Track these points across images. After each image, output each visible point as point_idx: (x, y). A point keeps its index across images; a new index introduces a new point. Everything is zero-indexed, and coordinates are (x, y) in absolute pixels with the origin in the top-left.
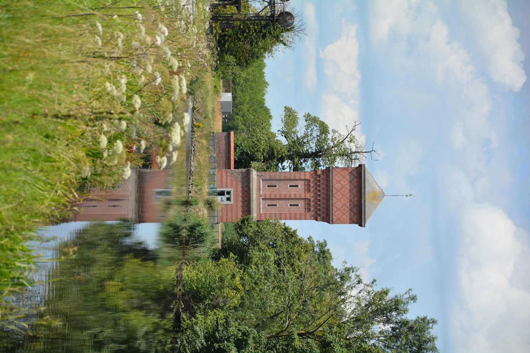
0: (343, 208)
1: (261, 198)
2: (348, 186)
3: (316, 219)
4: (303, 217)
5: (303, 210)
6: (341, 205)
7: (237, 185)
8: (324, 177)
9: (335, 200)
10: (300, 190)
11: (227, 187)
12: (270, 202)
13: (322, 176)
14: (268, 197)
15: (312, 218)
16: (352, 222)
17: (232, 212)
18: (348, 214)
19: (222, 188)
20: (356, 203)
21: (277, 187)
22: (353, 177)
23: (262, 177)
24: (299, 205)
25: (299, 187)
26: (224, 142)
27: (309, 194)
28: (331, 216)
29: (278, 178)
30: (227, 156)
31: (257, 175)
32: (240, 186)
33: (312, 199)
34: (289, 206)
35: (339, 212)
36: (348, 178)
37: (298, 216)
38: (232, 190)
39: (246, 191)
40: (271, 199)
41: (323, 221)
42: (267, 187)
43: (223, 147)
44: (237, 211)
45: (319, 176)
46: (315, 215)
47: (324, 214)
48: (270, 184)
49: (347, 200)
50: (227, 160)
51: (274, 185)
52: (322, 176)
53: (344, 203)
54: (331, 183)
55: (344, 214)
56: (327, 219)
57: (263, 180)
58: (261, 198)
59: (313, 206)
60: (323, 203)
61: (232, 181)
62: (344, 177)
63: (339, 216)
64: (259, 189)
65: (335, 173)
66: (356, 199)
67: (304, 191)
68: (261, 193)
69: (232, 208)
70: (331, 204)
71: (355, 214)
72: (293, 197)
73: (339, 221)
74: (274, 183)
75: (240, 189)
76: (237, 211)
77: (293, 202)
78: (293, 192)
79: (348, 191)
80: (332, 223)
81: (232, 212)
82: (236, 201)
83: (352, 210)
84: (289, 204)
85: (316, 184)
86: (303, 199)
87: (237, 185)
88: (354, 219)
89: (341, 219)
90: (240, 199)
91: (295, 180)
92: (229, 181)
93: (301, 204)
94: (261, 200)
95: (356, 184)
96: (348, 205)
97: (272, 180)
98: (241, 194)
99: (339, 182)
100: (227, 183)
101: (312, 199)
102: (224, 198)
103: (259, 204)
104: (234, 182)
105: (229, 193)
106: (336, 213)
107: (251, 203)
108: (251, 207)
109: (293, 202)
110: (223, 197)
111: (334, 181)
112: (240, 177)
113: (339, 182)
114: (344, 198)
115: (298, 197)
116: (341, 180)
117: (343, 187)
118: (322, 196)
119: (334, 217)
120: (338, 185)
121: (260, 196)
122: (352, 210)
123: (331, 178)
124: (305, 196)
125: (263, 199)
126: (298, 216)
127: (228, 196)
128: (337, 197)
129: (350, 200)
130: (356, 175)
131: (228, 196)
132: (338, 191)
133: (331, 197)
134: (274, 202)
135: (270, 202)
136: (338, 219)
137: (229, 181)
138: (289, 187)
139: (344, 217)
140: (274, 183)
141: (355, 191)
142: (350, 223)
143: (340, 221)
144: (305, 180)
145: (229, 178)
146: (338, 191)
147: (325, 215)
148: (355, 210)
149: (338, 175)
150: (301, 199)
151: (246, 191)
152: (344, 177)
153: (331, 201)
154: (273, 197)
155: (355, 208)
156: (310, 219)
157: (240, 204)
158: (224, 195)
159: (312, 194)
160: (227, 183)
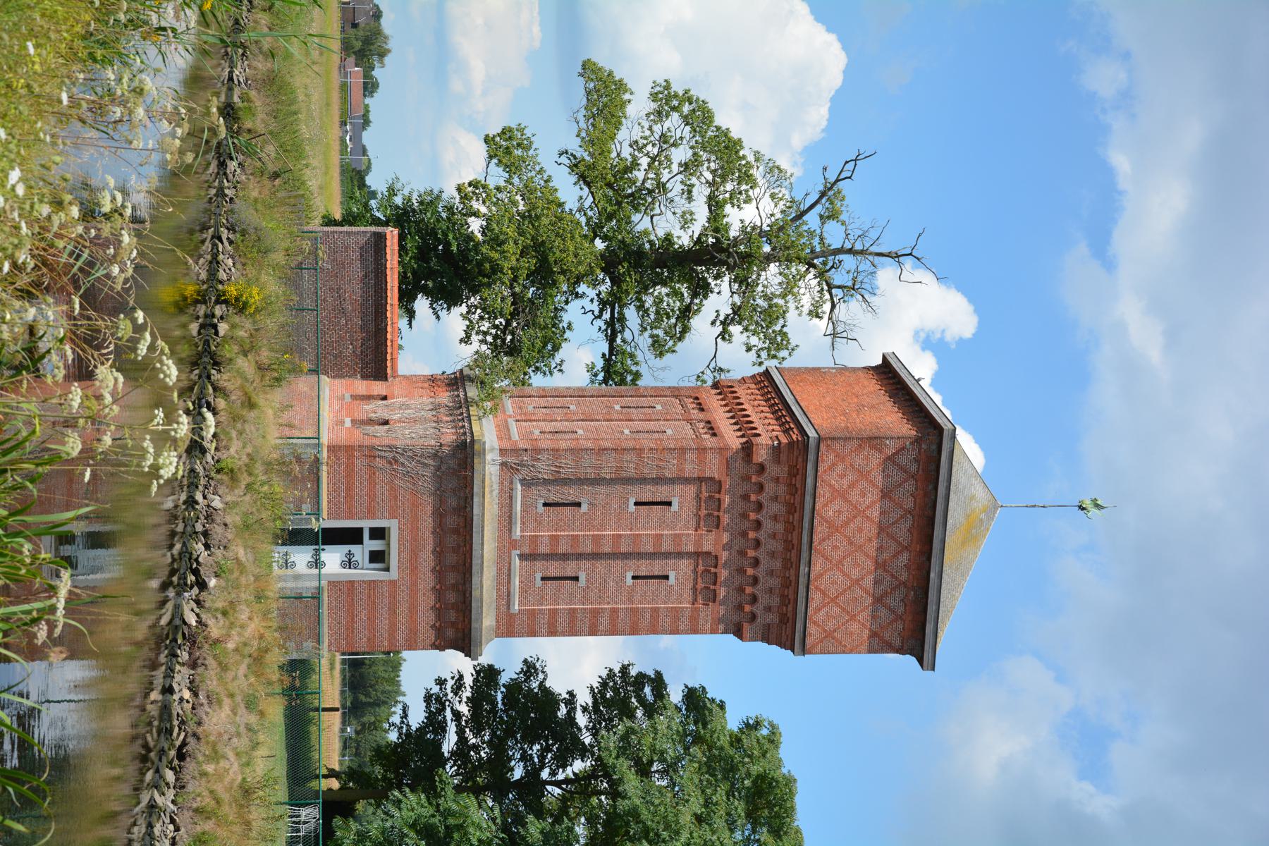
0: (849, 595)
1: (515, 553)
2: (874, 513)
3: (739, 633)
4: (685, 623)
5: (687, 594)
6: (843, 582)
7: (415, 506)
8: (783, 471)
9: (818, 565)
10: (679, 522)
11: (371, 514)
12: (552, 568)
13: (772, 469)
14: (544, 549)
15: (721, 627)
16: (879, 644)
17: (392, 610)
18: (865, 617)
19: (351, 516)
20: (903, 576)
21: (584, 508)
22: (898, 477)
23: (524, 472)
24: (672, 575)
25: (675, 507)
26: (356, 271)
27: (712, 536)
28: (799, 626)
29: (590, 473)
30: (372, 327)
31: (503, 464)
32: (429, 509)
33: (724, 556)
34: (629, 581)
35: (833, 609)
36: (877, 476)
37: (666, 621)
38: (393, 525)
39: (455, 531)
40: (559, 481)
41: (767, 639)
42: (541, 509)
43: (354, 290)
44: (413, 609)
45: (762, 468)
46: (734, 617)
47: (777, 618)
48: (553, 498)
49: (870, 565)
50: (371, 343)
51: (571, 499)
52: (772, 469)
53: (855, 574)
54: (808, 498)
55: (853, 618)
56: (786, 630)
57: (523, 481)
58: (515, 553)
59: (729, 491)
60: (772, 554)
61: (393, 490)
62: (865, 475)
63: (831, 626)
64: (507, 519)
65: (827, 458)
66: (904, 558)
67: (693, 522)
68: (517, 532)
69: (392, 596)
70: (802, 580)
71: (898, 617)
72: (646, 547)
73: (827, 643)
74: (570, 493)
75: (426, 522)
76: (413, 609)
77: (645, 568)
78: (649, 529)
79: (875, 530)
80: (804, 652)
81: (392, 610)
82: (411, 565)
83: (887, 600)
84: (629, 575)
85: (740, 607)
86: (688, 555)
87: (415, 506)
88: (891, 636)
89: (838, 635)
90: (427, 559)
91: (660, 480)
92: (382, 490)
93: (680, 573)
94: (517, 562)
95: (909, 504)
96: (869, 582)
97: (565, 482)
98: (430, 600)
99: (842, 494)
100: (372, 496)
101: (724, 556)
102: (360, 552)
103: (505, 577)
104: (403, 496)
105: (378, 533)
106: (820, 614)
107: (475, 580)
108: (475, 593)
109: (645, 568)
110: (355, 549)
111: (820, 491)
112: (428, 473)
113: (842, 494)
114: (858, 555)
115: (668, 547)
116: (852, 485)
117: (859, 512)
118: (768, 545)
119: (811, 628)
120: (839, 505)
121: (513, 544)
122: (887, 600)
123: (809, 481)
124: (698, 543)
125: (522, 557)
126: (666, 621)
127: (377, 545)
128: (829, 552)
129: (880, 565)
130: (913, 467)
131: (377, 545)
132: (834, 529)
133: (805, 555)
134: (568, 568)
135: (552, 568)
136: (828, 635)
137: (382, 490)
138: (632, 508)
139: (854, 627)
140: (570, 493)
141: (902, 530)
142: (872, 650)
143: (834, 644)
144: (700, 480)
145: (382, 477)
146: (834, 529)
147: (773, 618)
148: (896, 603)
149: (840, 468)
150: (679, 555)
151: (455, 531)
152: (865, 475)
153: (803, 569)
154: (565, 548)
155: (899, 595)
156: (714, 631)
157: (427, 581)
158: (360, 542)
159: (725, 537)
160: (372, 496)
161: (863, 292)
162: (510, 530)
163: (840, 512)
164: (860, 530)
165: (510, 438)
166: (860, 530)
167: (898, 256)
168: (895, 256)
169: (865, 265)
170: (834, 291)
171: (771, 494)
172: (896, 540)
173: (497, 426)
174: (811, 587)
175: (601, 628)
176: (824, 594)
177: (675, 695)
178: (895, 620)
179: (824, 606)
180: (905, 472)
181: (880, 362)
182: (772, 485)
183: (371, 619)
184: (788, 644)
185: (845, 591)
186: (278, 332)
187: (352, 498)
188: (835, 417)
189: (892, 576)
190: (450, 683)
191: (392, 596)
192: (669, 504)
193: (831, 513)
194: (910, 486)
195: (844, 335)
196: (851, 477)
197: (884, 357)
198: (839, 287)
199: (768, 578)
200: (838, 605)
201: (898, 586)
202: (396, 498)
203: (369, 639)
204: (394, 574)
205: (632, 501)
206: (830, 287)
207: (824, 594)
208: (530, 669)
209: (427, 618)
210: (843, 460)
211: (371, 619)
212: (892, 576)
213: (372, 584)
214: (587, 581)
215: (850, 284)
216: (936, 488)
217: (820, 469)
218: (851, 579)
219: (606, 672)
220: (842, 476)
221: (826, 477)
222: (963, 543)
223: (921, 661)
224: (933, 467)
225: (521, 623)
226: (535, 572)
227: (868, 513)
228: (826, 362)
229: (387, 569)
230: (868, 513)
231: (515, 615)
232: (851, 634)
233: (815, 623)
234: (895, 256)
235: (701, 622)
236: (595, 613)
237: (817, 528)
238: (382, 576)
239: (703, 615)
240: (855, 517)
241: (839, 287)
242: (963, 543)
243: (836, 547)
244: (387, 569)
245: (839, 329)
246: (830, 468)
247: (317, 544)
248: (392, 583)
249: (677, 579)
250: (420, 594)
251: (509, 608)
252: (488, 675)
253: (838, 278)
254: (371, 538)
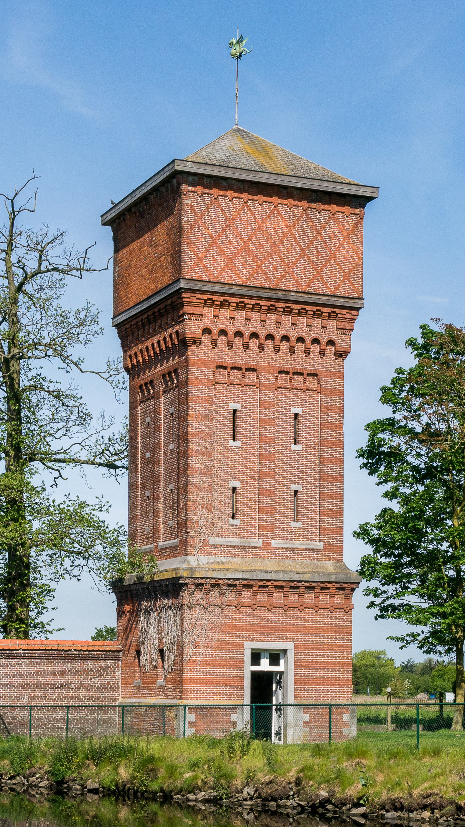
0: (314, 258)
6: (303, 263)
11: (240, 664)
17: (318, 647)
19: (242, 681)
20: (298, 211)
25: (237, 406)
35: (326, 272)
38: (250, 646)
44: (318, 630)
55: (333, 256)
63: (339, 275)
69: (308, 647)
73: (353, 279)
76: (318, 630)
81: (318, 647)
99: (230, 261)
111: (226, 279)
113: (230, 261)
116: (222, 252)
119: (341, 292)
120: (238, 263)
132: (259, 269)
136: (346, 278)
146: (259, 269)
157: (295, 618)
161: (45, 243)
162: (255, 548)
163: (244, 263)
164: (260, 246)
165: (177, 547)
166: (260, 246)
167: (14, 212)
168: (14, 215)
169: (23, 240)
170: (43, 269)
171: (228, 322)
172: (269, 216)
173: (165, 557)
174: (307, 290)
175: (337, 472)
176: (313, 279)
177: (386, 412)
178: (336, 219)
179: (323, 280)
180: (211, 205)
181: (109, 229)
182: (220, 321)
183: (326, 665)
184: (353, 312)
185: (310, 261)
186: (317, 794)
187: (226, 680)
188: (162, 266)
189: (298, 220)
190: (371, 598)
191: (308, 647)
192: (235, 411)
193: (245, 271)
194: (223, 202)
195: (81, 261)
196: (214, 251)
197: (105, 224)
198: (40, 265)
199: (298, 327)
200: (322, 269)
201: (308, 216)
202: (227, 643)
203: (342, 667)
204: (289, 646)
205: (231, 443)
206: (39, 272)
207: (313, 279)
208: (363, 532)
209: (325, 619)
210: (200, 259)
211: (326, 665)
212: (298, 220)
213: (297, 664)
214: (298, 483)
215: (37, 254)
216: (226, 179)
217: (207, 279)
218: (301, 256)
219: (364, 469)
220: (214, 260)
221: (215, 274)
222: (270, 158)
223: (370, 199)
224: (206, 180)
225: (331, 539)
226: (290, 527)
227: (245, 239)
228: (109, 275)
229: (285, 651)
230: (245, 239)
231: (325, 545)
232: (346, 258)
233: (337, 289)
234: (14, 215)
235: (334, 386)
236: (323, 477)
237: (258, 283)
238: (291, 655)
239: (328, 385)
240: (249, 250)
241: (40, 265)
242: (270, 158)
243: (274, 268)
244: (285, 651)
245: (75, 264)
246: (207, 271)
247: (270, 708)
248: (296, 647)
249: (298, 406)
250: (306, 624)
251: (319, 550)
252: (368, 568)
253: (32, 264)
254: (258, 664)
